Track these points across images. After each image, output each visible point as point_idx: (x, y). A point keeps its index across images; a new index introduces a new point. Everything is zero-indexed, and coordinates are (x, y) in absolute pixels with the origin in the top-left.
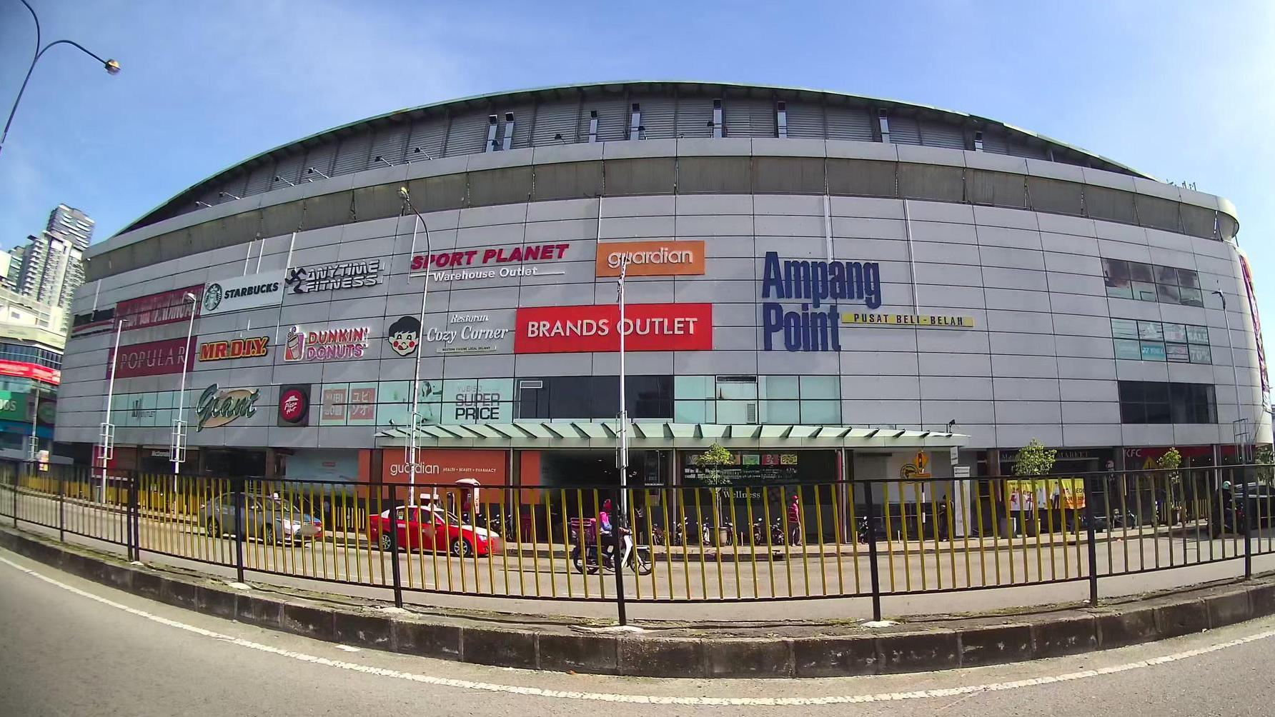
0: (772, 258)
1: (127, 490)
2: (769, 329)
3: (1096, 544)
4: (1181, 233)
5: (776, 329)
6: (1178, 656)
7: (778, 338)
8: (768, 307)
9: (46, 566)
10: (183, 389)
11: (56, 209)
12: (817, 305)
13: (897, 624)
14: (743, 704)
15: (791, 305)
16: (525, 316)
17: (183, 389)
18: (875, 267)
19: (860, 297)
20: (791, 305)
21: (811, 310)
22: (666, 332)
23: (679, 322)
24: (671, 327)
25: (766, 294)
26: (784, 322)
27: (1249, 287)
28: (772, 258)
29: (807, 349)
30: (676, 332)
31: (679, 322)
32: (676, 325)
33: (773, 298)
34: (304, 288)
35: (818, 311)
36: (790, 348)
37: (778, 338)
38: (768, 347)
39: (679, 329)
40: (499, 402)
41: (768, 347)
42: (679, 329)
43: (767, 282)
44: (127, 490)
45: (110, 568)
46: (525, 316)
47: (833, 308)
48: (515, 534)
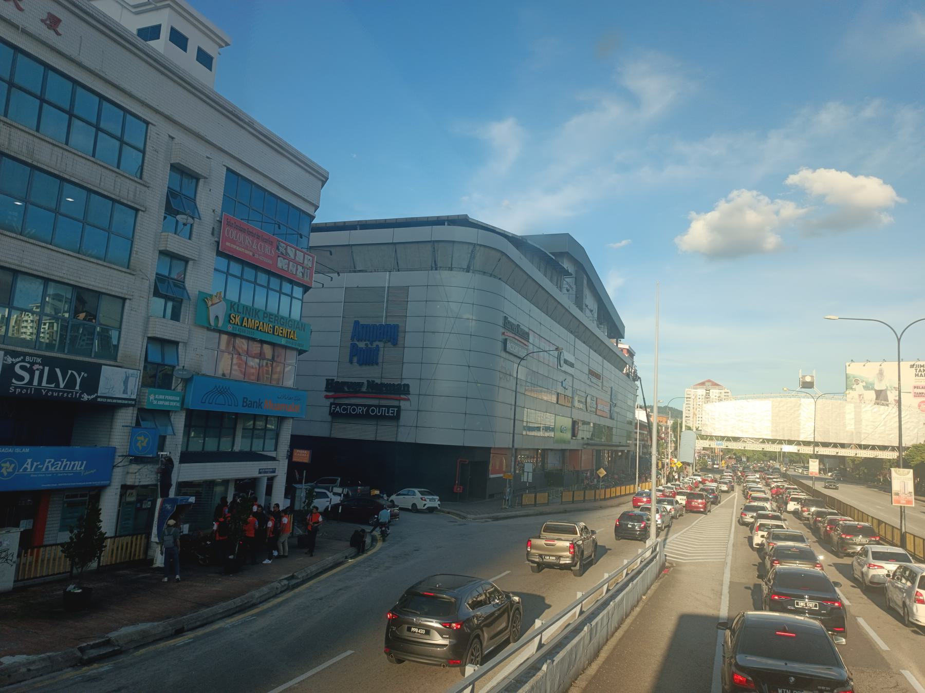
0: (357, 323)
1: (33, 367)
4: (865, 514)
14: (358, 287)
15: (362, 345)
16: (260, 469)
20: (362, 345)
22: (386, 414)
23: (392, 410)
24: (388, 413)
27: (736, 439)
28: (357, 323)
30: (390, 415)
31: (392, 410)
32: (390, 412)
34: (138, 480)
39: (391, 413)
40: (519, 364)
42: (391, 413)
44: (33, 367)
46: (260, 469)
48: (538, 427)
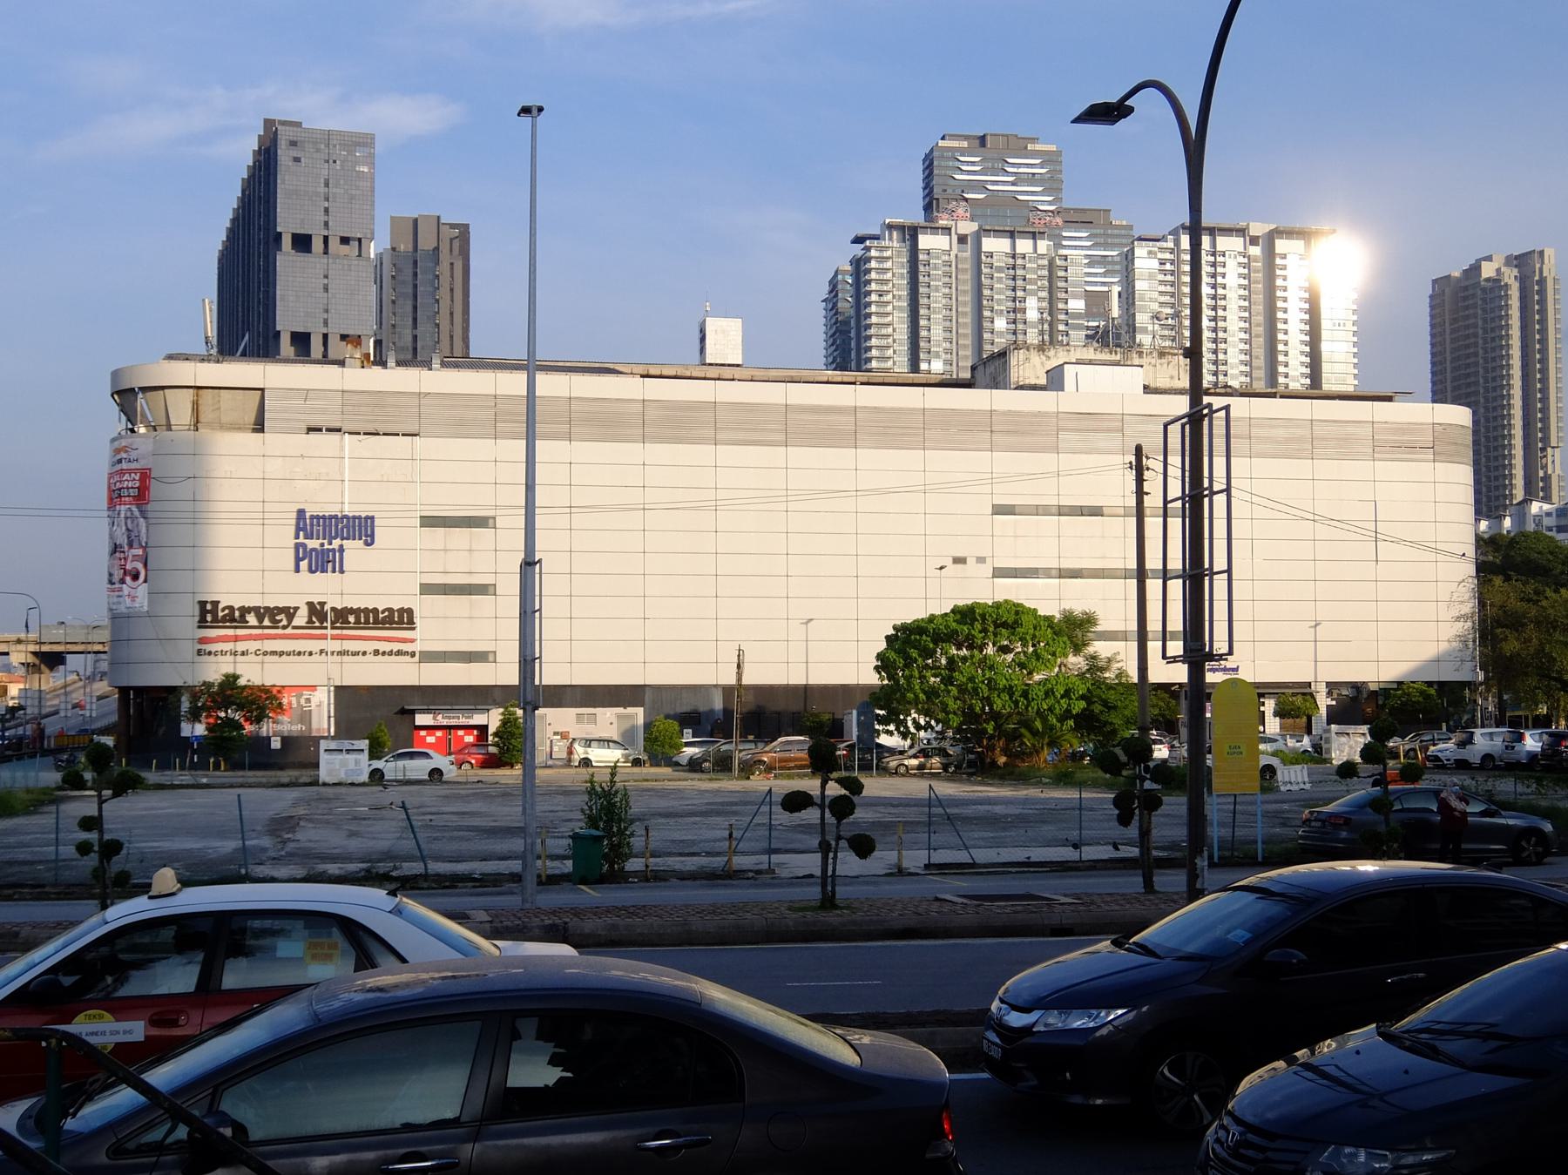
0: (301, 513)
2: (298, 560)
3: (1182, 653)
5: (303, 559)
6: (685, 984)
7: (304, 564)
8: (297, 546)
9: (239, 1121)
10: (347, 459)
11: (932, 150)
12: (330, 544)
13: (979, 905)
15: (313, 544)
17: (347, 456)
18: (372, 518)
19: (360, 539)
20: (313, 544)
21: (326, 546)
25: (297, 537)
26: (308, 553)
29: (322, 572)
33: (301, 540)
35: (330, 547)
36: (311, 571)
37: (304, 564)
38: (297, 570)
41: (297, 570)
43: (298, 529)
45: (1402, 855)
47: (341, 546)
